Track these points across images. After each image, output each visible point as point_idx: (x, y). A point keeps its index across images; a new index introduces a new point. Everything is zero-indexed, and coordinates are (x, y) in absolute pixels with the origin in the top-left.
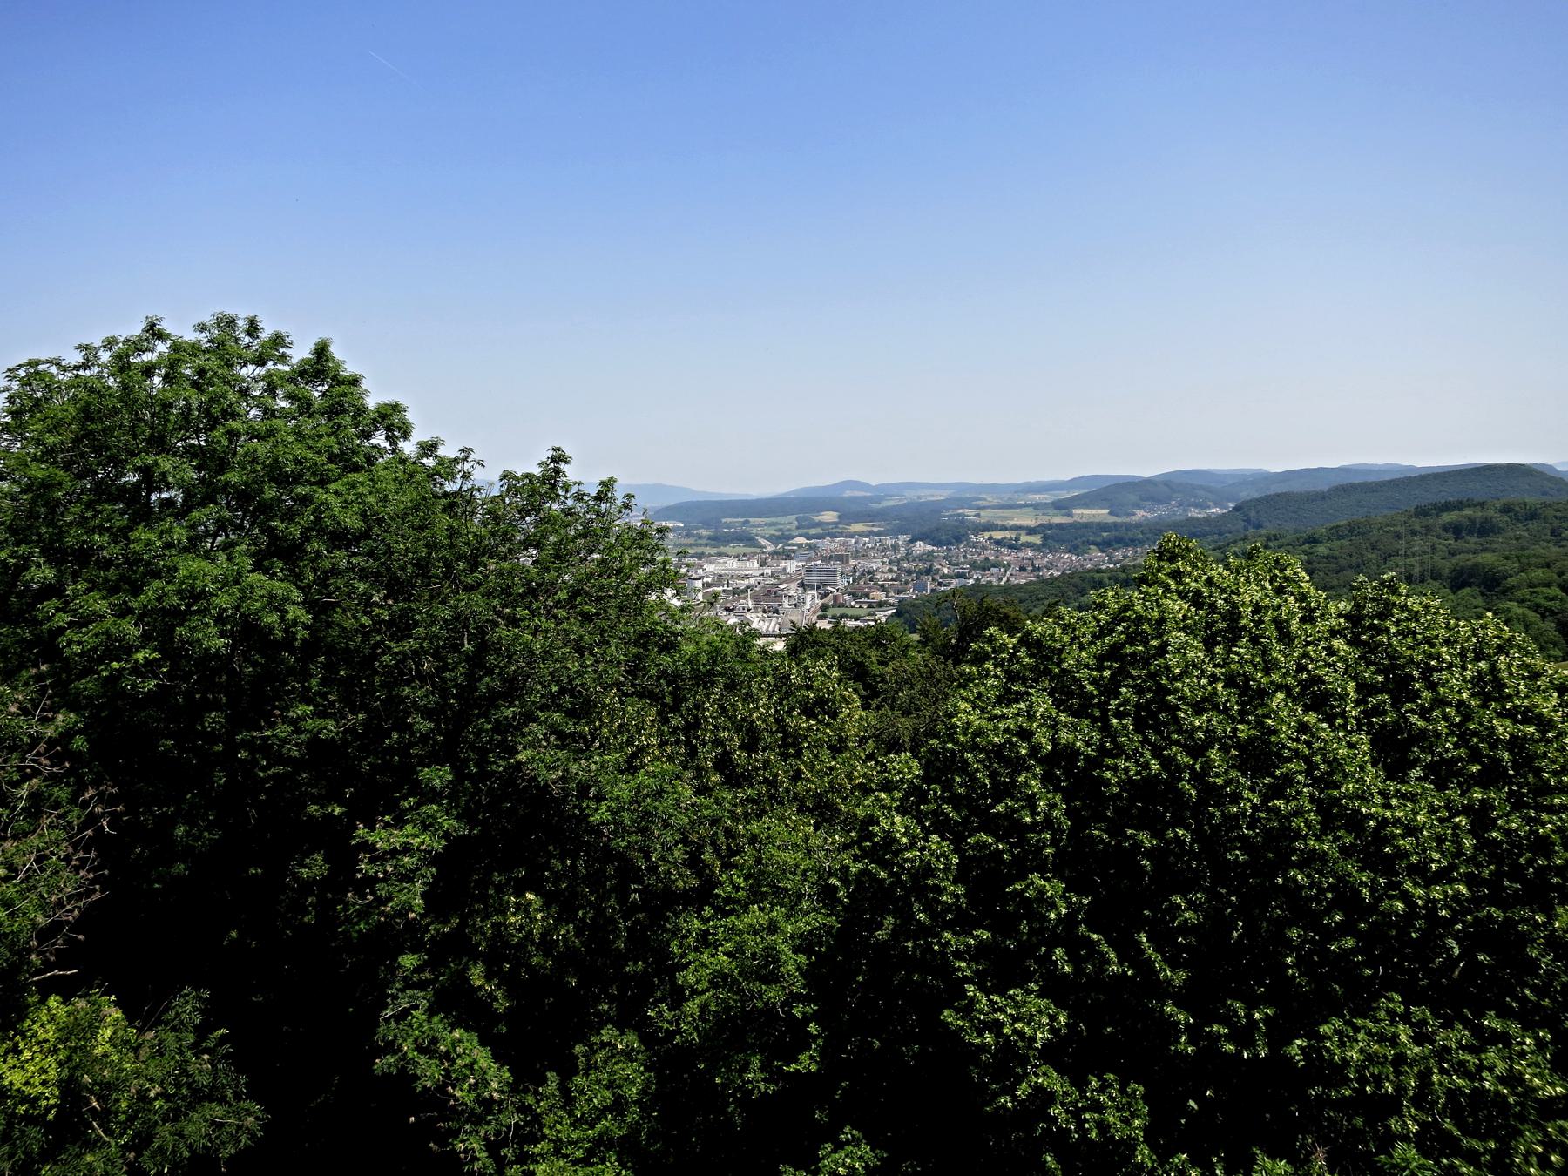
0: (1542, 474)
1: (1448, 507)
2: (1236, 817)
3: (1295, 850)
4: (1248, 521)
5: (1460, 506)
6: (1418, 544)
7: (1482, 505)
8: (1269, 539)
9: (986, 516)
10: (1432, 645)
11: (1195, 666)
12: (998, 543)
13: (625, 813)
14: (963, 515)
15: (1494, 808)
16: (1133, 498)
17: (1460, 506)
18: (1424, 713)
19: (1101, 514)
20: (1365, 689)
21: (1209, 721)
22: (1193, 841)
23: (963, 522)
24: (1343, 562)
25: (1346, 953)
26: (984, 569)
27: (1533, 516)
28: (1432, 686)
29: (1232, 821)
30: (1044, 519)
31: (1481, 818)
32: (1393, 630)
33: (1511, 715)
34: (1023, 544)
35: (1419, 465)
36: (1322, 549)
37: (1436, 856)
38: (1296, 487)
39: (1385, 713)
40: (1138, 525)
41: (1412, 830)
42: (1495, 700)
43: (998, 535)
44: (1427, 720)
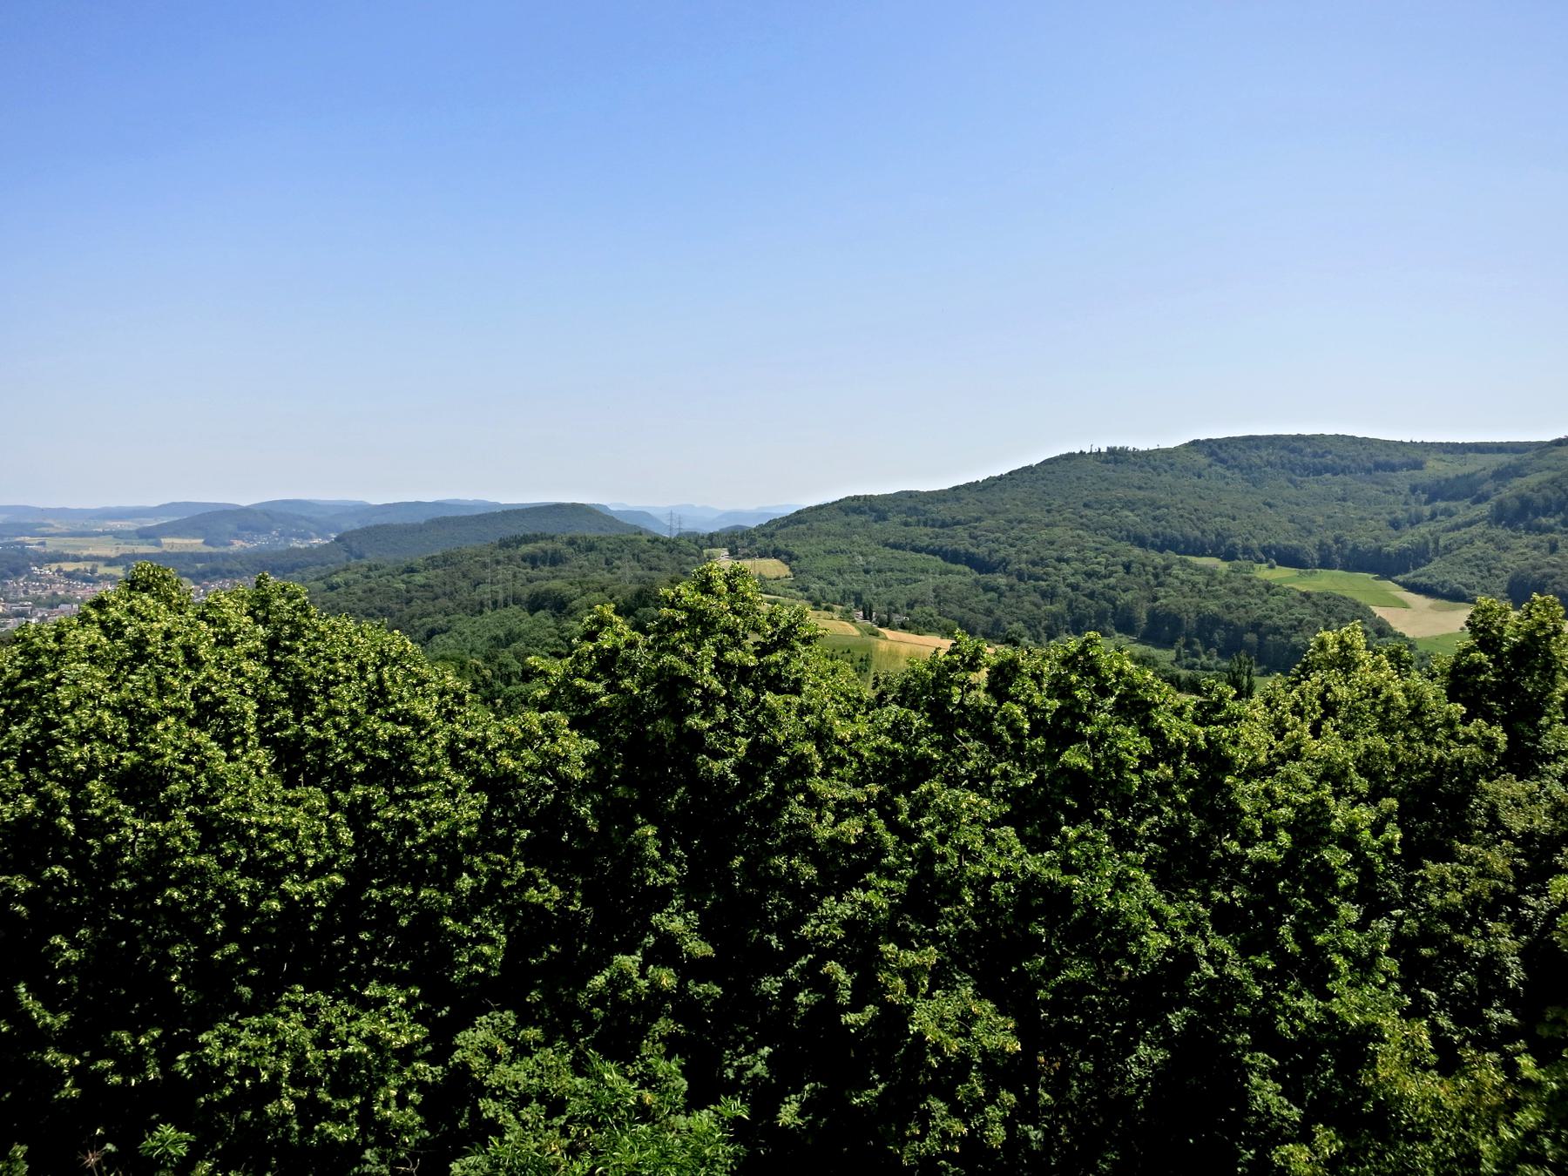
0: (598, 513)
1: (526, 540)
2: (118, 845)
3: (174, 869)
4: (350, 551)
5: (535, 538)
6: (503, 572)
7: (552, 538)
8: (370, 569)
9: (52, 545)
10: (332, 661)
11: (90, 697)
12: (69, 575)
13: (1354, 917)
14: (23, 544)
15: (374, 801)
16: (231, 527)
17: (535, 538)
18: (317, 723)
19: (195, 544)
20: (265, 706)
21: (92, 750)
22: (71, 877)
23: (23, 552)
24: (438, 590)
25: (229, 959)
26: (52, 607)
27: (591, 548)
28: (328, 697)
29: (115, 851)
30: (126, 549)
31: (359, 814)
32: (302, 649)
33: (393, 718)
34: (101, 577)
35: (377, 499)
36: (419, 579)
37: (312, 852)
38: (396, 519)
39: (287, 727)
40: (236, 556)
41: (289, 833)
42: (381, 706)
43: (69, 567)
44: (320, 730)
